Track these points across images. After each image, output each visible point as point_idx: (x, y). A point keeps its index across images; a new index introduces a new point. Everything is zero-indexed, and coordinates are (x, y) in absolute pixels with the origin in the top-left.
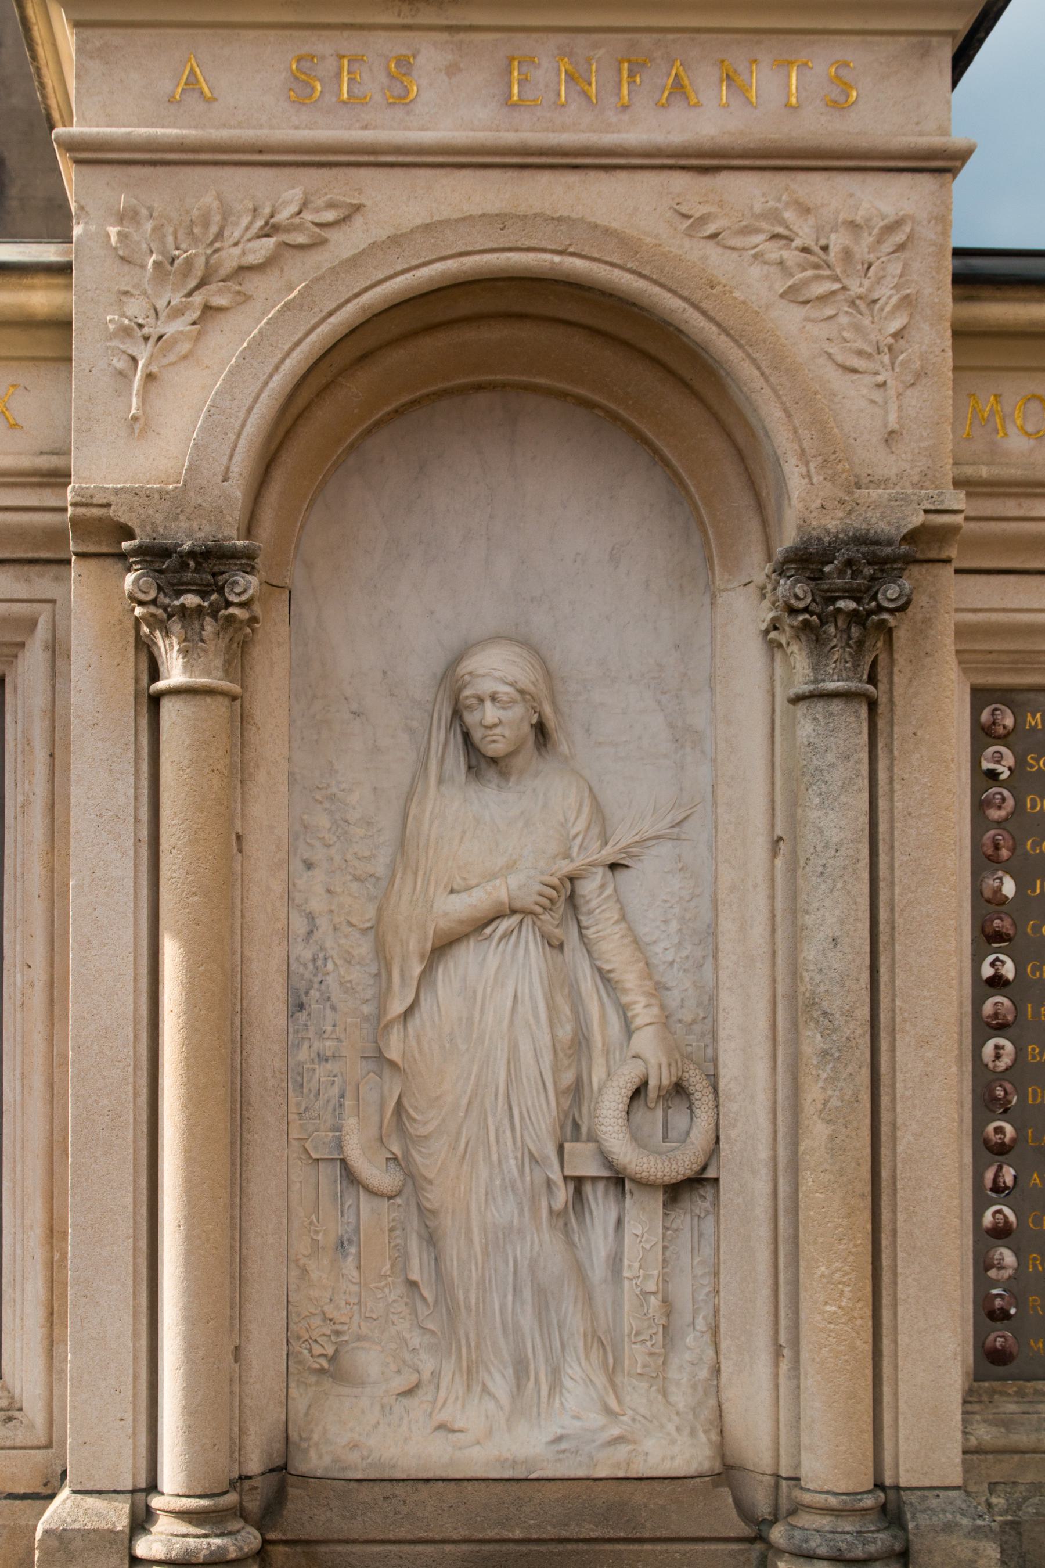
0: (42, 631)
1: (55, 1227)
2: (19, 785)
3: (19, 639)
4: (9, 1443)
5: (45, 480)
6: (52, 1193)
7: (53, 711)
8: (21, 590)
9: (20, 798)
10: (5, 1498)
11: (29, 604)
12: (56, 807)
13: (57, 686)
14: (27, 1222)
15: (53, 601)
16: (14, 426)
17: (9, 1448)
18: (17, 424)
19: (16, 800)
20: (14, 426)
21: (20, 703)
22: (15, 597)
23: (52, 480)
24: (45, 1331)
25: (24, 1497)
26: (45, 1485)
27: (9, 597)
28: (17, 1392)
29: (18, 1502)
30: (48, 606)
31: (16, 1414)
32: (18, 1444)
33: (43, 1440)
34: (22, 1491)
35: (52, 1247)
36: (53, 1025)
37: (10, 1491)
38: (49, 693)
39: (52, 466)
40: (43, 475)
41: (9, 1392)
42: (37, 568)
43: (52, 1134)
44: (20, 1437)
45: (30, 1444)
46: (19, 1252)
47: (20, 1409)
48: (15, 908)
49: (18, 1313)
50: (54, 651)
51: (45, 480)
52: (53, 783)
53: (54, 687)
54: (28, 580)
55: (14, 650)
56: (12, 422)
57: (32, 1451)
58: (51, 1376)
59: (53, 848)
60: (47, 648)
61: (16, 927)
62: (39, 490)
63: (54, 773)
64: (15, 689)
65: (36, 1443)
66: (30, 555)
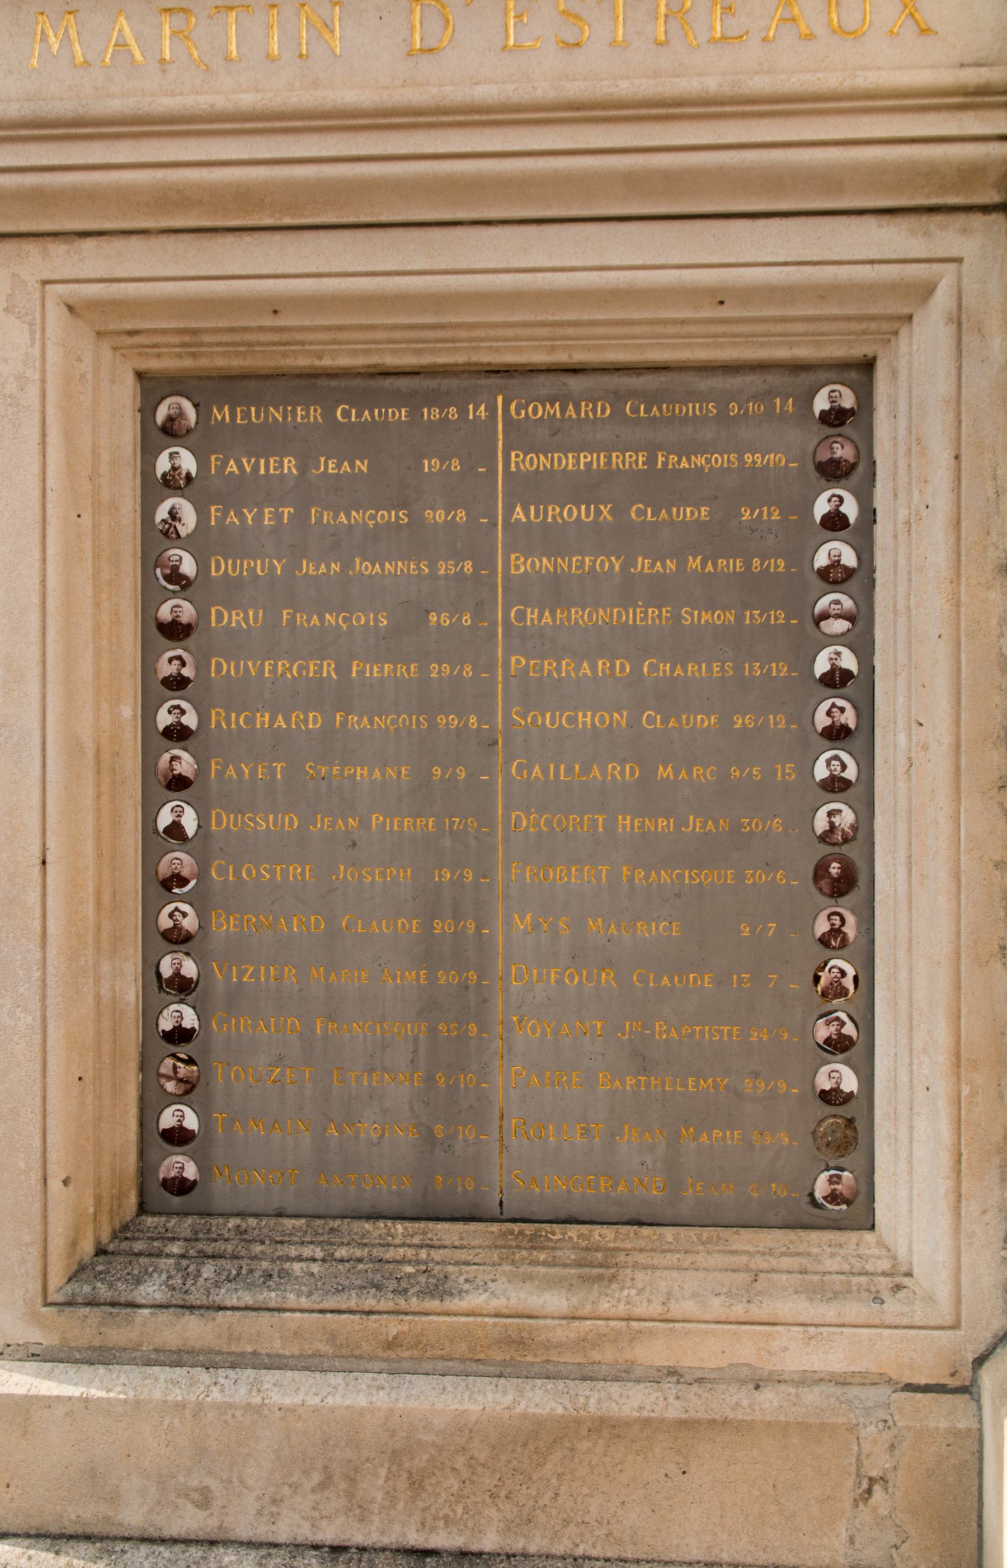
0: (942, 298)
1: (963, 1053)
2: (902, 495)
3: (906, 311)
4: (905, 1321)
5: (969, 100)
6: (959, 1010)
7: (959, 402)
8: (918, 248)
9: (903, 513)
10: (903, 1390)
11: (927, 265)
12: (964, 524)
13: (965, 368)
14: (918, 1044)
15: (959, 260)
16: (925, 31)
17: (905, 1327)
18: (929, 29)
19: (896, 514)
20: (925, 31)
21: (903, 392)
22: (911, 255)
23: (979, 100)
24: (950, 1183)
25: (926, 1389)
26: (953, 1375)
27: (902, 256)
28: (902, 1252)
29: (919, 1396)
30: (952, 267)
31: (906, 1281)
32: (917, 1321)
33: (949, 1319)
34: (923, 1381)
35: (959, 1079)
36: (959, 799)
37: (909, 1381)
38: (954, 378)
39: (983, 80)
40: (967, 94)
41: (889, 1250)
42: (939, 218)
43: (958, 937)
44: (919, 1314)
45: (932, 1323)
46: (904, 1078)
47: (909, 1274)
48: (895, 650)
49: (903, 1154)
50: (959, 325)
51: (969, 100)
52: (959, 492)
53: (959, 369)
54: (927, 234)
55: (895, 326)
56: (924, 27)
57: (936, 1333)
58: (958, 1239)
59: (958, 575)
60: (950, 319)
61: (896, 675)
62: (958, 115)
63: (959, 480)
64: (894, 374)
65: (939, 1322)
66: (933, 201)
